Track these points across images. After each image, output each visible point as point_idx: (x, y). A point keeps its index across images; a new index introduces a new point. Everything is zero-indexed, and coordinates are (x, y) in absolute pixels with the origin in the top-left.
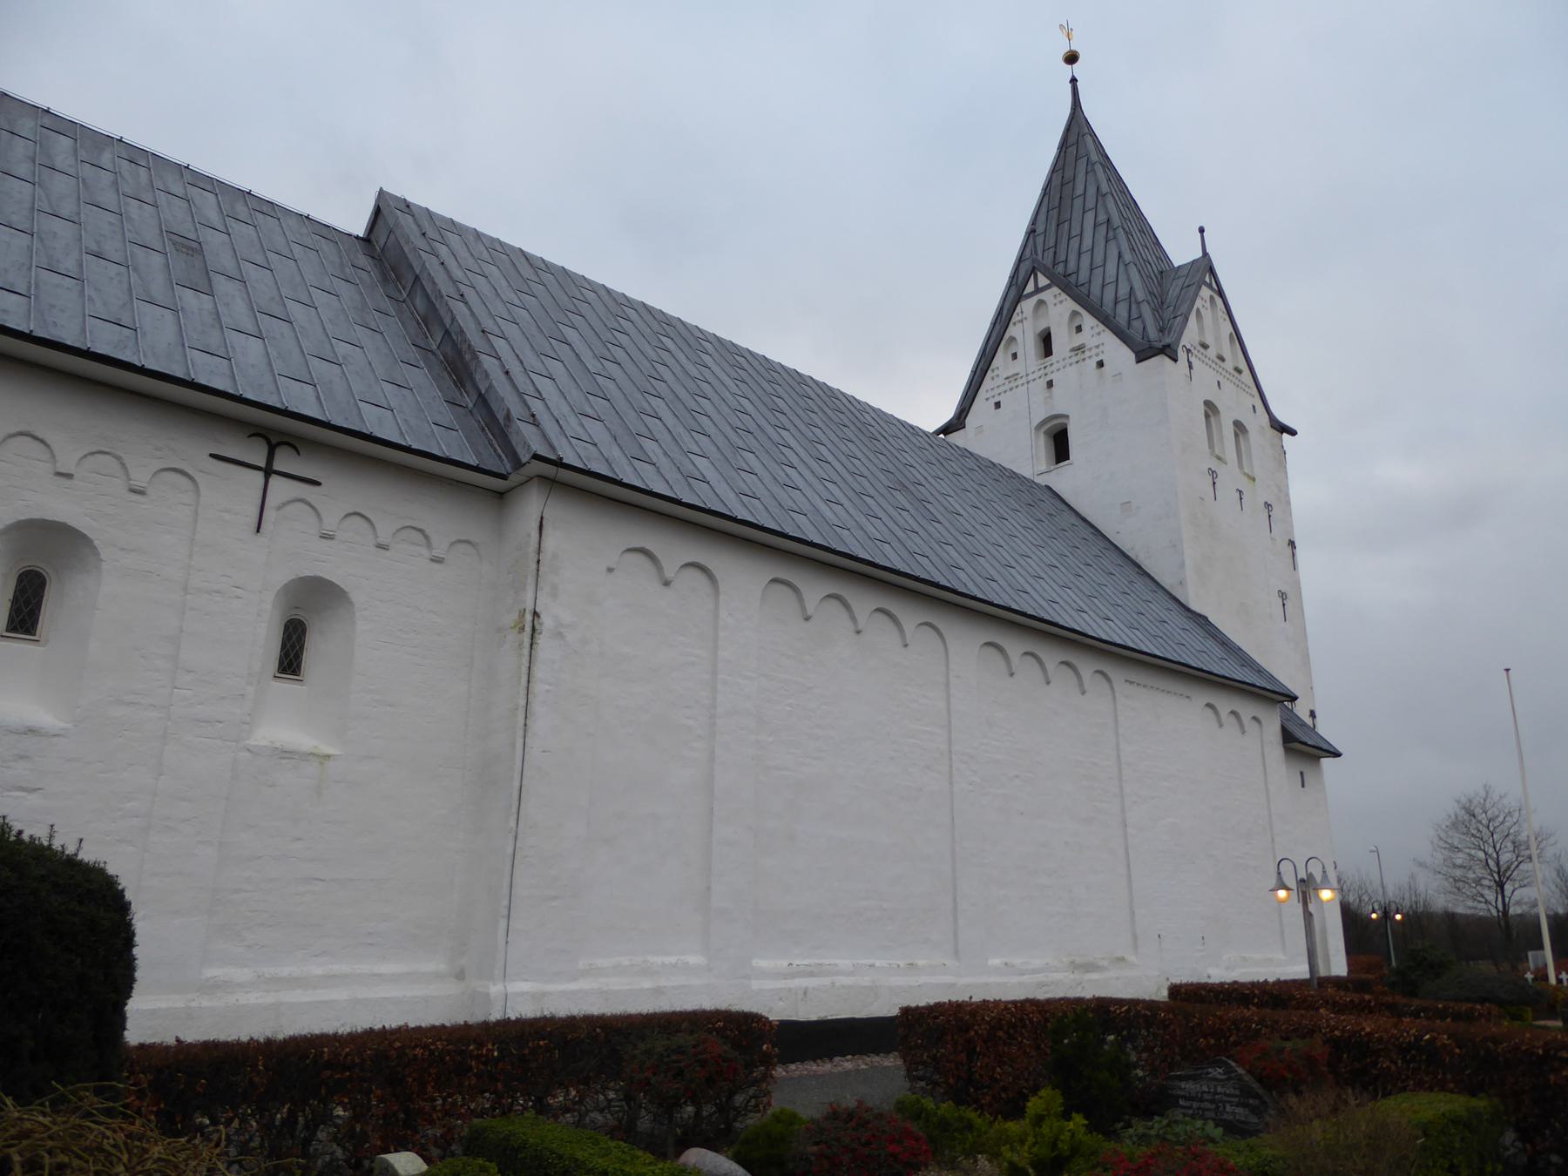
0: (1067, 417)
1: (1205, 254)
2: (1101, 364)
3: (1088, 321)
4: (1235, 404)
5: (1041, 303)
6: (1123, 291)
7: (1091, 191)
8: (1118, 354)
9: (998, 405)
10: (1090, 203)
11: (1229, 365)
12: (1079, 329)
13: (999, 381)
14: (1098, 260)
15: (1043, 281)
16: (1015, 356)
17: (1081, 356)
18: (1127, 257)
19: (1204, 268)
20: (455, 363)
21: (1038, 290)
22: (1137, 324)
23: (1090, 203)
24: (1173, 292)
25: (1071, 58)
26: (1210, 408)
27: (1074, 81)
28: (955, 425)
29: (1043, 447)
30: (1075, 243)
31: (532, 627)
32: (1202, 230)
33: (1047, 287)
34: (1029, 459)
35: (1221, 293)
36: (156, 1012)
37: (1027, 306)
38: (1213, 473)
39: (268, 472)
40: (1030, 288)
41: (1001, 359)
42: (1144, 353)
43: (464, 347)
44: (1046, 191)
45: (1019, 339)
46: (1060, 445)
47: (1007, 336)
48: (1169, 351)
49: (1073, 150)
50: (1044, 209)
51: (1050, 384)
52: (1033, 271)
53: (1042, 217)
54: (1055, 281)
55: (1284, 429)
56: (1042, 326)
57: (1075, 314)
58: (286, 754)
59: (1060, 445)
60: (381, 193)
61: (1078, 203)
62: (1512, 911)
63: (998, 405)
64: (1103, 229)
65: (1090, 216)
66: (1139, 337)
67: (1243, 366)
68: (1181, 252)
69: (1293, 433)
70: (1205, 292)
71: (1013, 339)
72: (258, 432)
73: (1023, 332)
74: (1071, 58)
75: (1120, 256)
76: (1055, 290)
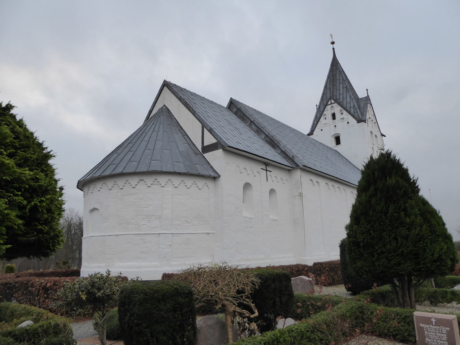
1: (368, 96)
2: (348, 123)
3: (345, 112)
4: (375, 132)
5: (332, 106)
6: (352, 105)
7: (341, 79)
8: (353, 121)
9: (322, 130)
10: (341, 82)
11: (373, 122)
12: (342, 114)
13: (321, 124)
14: (345, 96)
15: (333, 102)
16: (325, 119)
17: (343, 120)
18: (352, 97)
19: (367, 99)
20: (273, 143)
21: (331, 104)
22: (356, 114)
23: (341, 82)
24: (362, 104)
25: (333, 43)
26: (371, 132)
27: (333, 49)
28: (311, 133)
29: (334, 141)
30: (338, 91)
31: (301, 195)
32: (367, 90)
34: (331, 143)
35: (371, 105)
37: (329, 107)
38: (373, 148)
39: (266, 170)
40: (329, 103)
41: (322, 119)
42: (359, 121)
43: (274, 140)
44: (329, 77)
45: (327, 114)
46: (338, 140)
47: (324, 114)
48: (365, 121)
49: (335, 67)
50: (329, 81)
51: (335, 126)
52: (330, 99)
53: (328, 84)
54: (336, 101)
55: (383, 135)
56: (333, 112)
57: (341, 110)
58: (274, 220)
59: (338, 140)
60: (231, 98)
61: (338, 81)
63: (322, 130)
64: (345, 89)
65: (341, 85)
66: (357, 117)
68: (361, 94)
69: (385, 136)
70: (369, 105)
71: (325, 114)
72: (266, 164)
74: (333, 43)
75: (350, 96)
76: (336, 104)
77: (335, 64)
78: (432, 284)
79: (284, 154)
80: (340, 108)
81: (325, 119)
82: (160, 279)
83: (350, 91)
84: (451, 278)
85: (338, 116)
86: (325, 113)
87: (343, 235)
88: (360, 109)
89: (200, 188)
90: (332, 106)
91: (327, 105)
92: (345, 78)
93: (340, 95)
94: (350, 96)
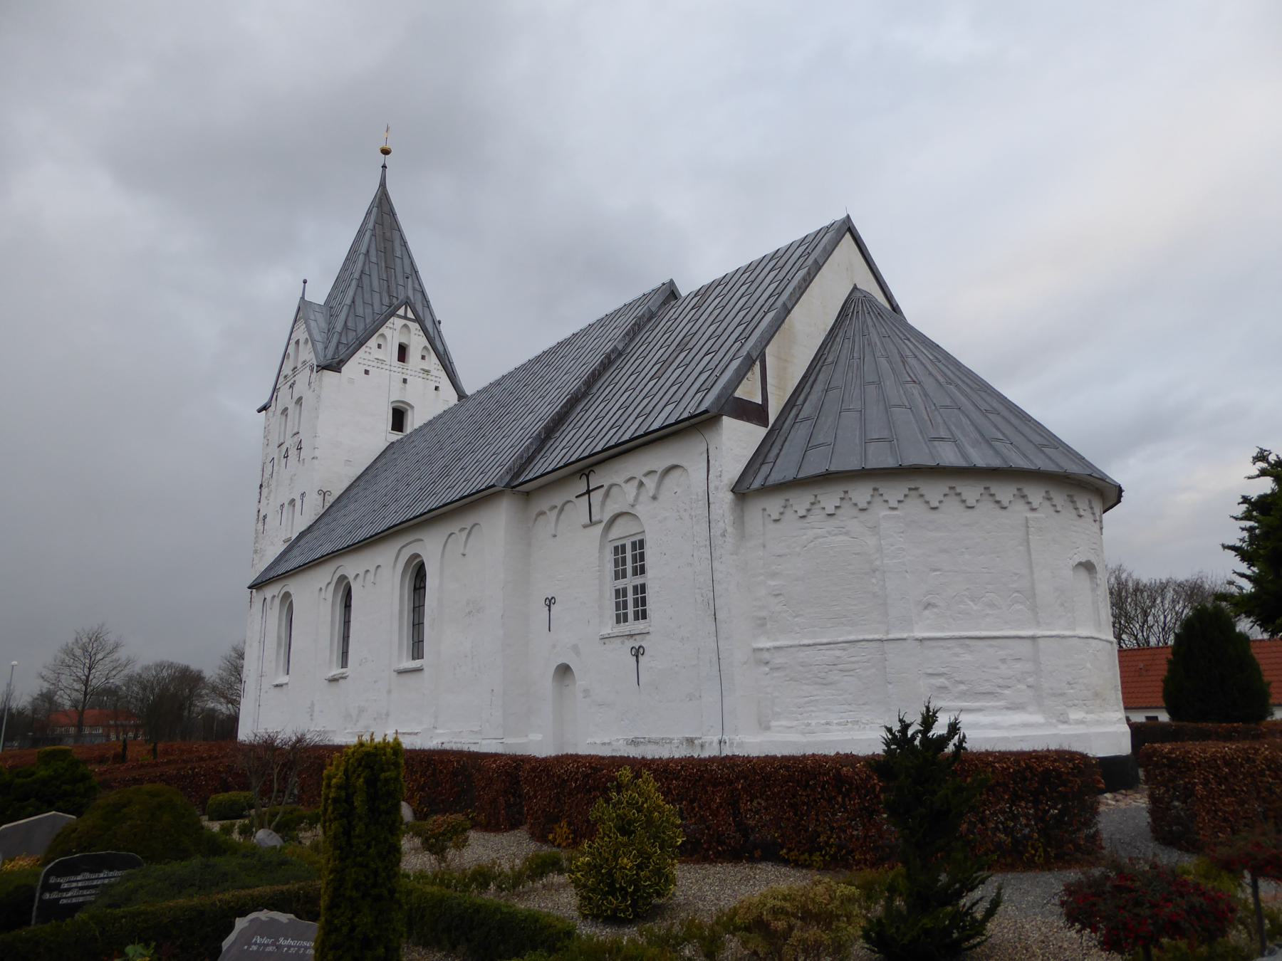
9: (367, 372)
21: (405, 317)
27: (384, 167)
37: (397, 322)
47: (380, 331)
51: (405, 381)
71: (382, 335)
74: (386, 152)
77: (382, 222)
78: (979, 944)
79: (1003, 434)
80: (425, 342)
86: (383, 330)
87: (649, 757)
89: (936, 504)
90: (405, 326)
91: (393, 314)
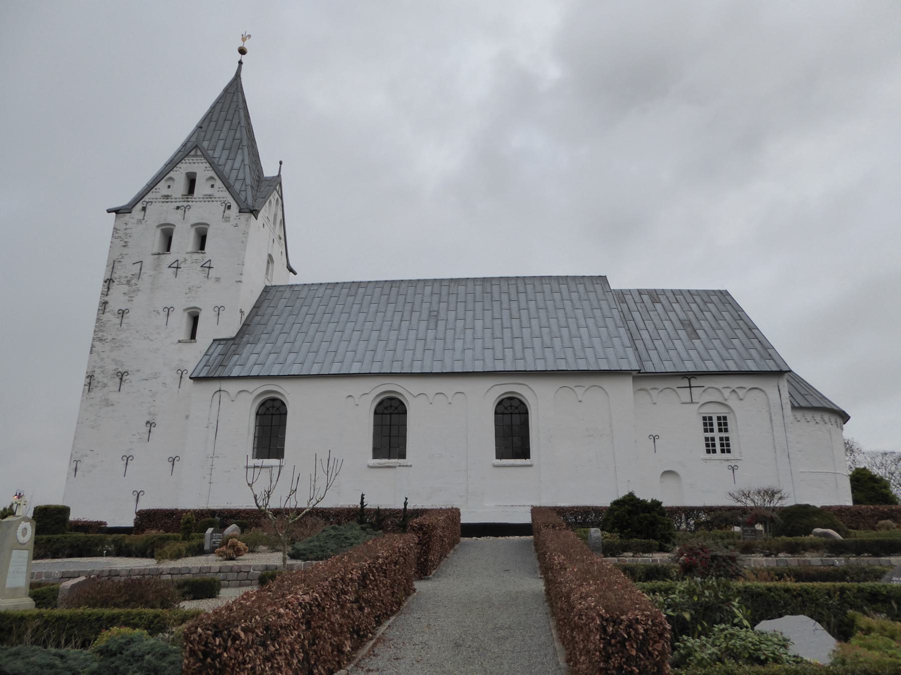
0: (208, 225)
1: (279, 175)
3: (218, 183)
15: (199, 153)
16: (169, 187)
19: (276, 181)
22: (243, 193)
27: (240, 63)
32: (281, 163)
33: (199, 156)
36: (73, 517)
39: (690, 387)
40: (193, 153)
41: (162, 185)
48: (254, 212)
62: (408, 507)
67: (283, 237)
68: (269, 171)
69: (295, 274)
73: (179, 176)
75: (243, 160)
77: (234, 89)
81: (169, 187)
82: (609, 505)
83: (246, 150)
84: (113, 574)
85: (201, 188)
88: (255, 192)
92: (241, 106)
93: (217, 121)
94: (243, 160)
